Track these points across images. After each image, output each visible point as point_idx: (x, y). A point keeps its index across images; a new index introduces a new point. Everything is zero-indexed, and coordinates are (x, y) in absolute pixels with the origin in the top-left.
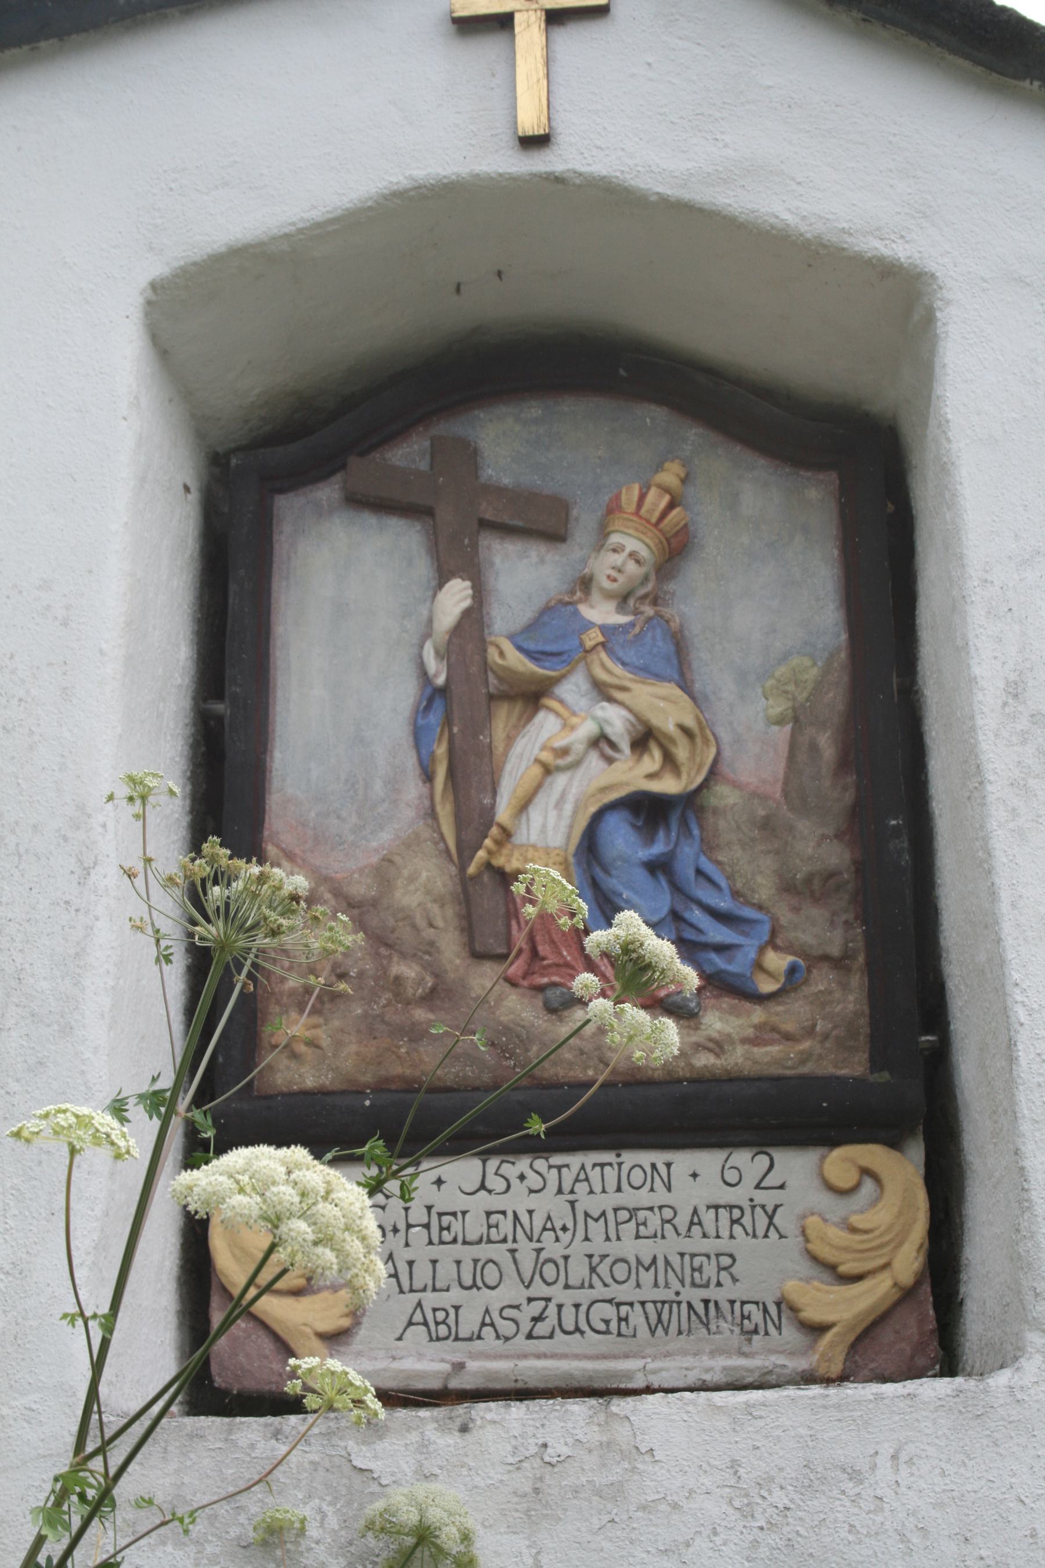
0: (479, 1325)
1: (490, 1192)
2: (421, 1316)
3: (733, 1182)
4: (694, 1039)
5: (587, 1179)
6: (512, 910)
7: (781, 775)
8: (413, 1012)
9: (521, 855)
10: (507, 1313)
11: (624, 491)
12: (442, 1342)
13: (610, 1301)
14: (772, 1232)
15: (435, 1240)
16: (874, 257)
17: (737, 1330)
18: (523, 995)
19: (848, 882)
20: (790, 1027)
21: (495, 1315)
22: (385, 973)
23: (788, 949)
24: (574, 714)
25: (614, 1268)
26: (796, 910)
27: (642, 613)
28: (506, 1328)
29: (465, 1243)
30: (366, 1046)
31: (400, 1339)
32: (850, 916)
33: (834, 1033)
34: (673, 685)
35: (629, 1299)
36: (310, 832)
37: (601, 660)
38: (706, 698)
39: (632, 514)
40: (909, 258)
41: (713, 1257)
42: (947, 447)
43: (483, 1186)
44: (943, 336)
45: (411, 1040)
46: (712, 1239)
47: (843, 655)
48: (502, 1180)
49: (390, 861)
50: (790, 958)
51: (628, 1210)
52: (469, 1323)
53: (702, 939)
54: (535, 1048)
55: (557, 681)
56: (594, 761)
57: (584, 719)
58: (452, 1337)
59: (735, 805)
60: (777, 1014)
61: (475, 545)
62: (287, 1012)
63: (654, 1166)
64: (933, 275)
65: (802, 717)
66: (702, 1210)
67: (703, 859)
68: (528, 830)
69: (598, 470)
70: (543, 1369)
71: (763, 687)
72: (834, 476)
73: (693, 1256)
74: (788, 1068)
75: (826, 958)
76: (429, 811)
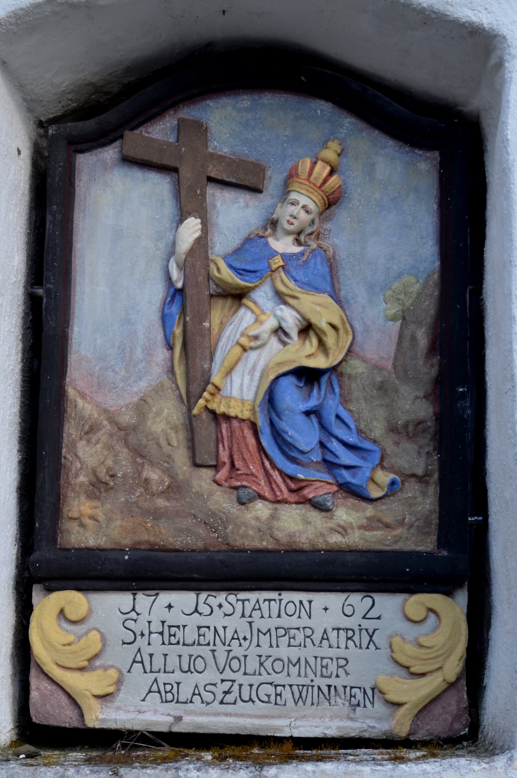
0: (191, 694)
1: (200, 614)
2: (156, 687)
3: (349, 614)
4: (330, 525)
5: (260, 609)
6: (220, 437)
7: (392, 355)
8: (156, 501)
9: (226, 403)
10: (208, 688)
11: (300, 164)
12: (169, 703)
13: (271, 684)
14: (372, 646)
15: (166, 642)
16: (467, 22)
17: (347, 704)
18: (225, 492)
19: (431, 427)
20: (388, 519)
21: (201, 689)
22: (139, 475)
23: (391, 469)
24: (263, 313)
25: (274, 664)
26: (397, 444)
27: (309, 246)
28: (208, 697)
29: (184, 644)
30: (126, 521)
31: (143, 700)
32: (430, 449)
33: (416, 524)
34: (326, 295)
35: (282, 683)
36: (95, 380)
37: (281, 277)
38: (348, 301)
39: (305, 179)
40: (490, 24)
41: (335, 660)
42: (506, 157)
43: (196, 610)
44: (509, 80)
45: (154, 519)
46: (334, 649)
47: (436, 276)
48: (208, 607)
49: (145, 401)
50: (392, 476)
51: (284, 629)
52: (185, 693)
53: (337, 461)
54: (231, 527)
55: (253, 289)
56: (274, 343)
57: (269, 317)
58: (175, 700)
59: (363, 373)
60: (381, 511)
61: (203, 195)
62: (78, 497)
63: (301, 602)
64: (504, 37)
65: (407, 318)
66: (329, 630)
67: (341, 408)
68: (231, 388)
69: (285, 145)
70: (229, 723)
71: (384, 296)
72: (437, 154)
73: (322, 658)
74: (387, 545)
75: (413, 475)
76: (171, 369)
